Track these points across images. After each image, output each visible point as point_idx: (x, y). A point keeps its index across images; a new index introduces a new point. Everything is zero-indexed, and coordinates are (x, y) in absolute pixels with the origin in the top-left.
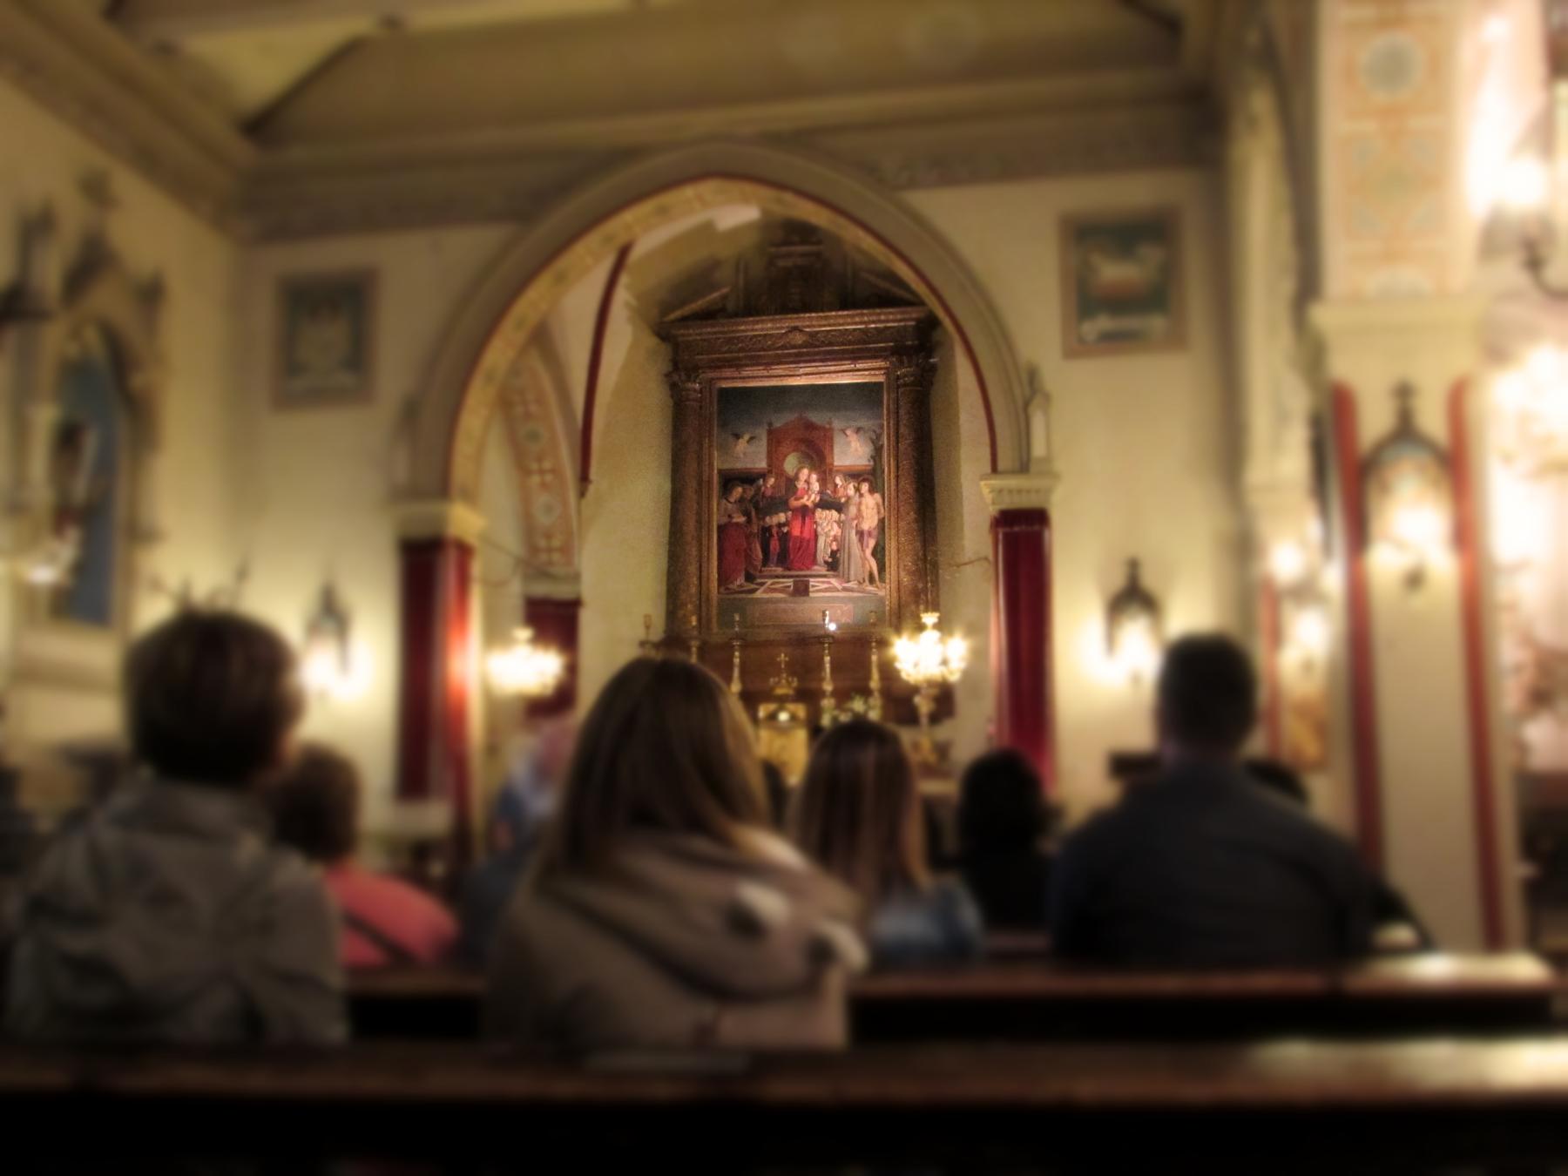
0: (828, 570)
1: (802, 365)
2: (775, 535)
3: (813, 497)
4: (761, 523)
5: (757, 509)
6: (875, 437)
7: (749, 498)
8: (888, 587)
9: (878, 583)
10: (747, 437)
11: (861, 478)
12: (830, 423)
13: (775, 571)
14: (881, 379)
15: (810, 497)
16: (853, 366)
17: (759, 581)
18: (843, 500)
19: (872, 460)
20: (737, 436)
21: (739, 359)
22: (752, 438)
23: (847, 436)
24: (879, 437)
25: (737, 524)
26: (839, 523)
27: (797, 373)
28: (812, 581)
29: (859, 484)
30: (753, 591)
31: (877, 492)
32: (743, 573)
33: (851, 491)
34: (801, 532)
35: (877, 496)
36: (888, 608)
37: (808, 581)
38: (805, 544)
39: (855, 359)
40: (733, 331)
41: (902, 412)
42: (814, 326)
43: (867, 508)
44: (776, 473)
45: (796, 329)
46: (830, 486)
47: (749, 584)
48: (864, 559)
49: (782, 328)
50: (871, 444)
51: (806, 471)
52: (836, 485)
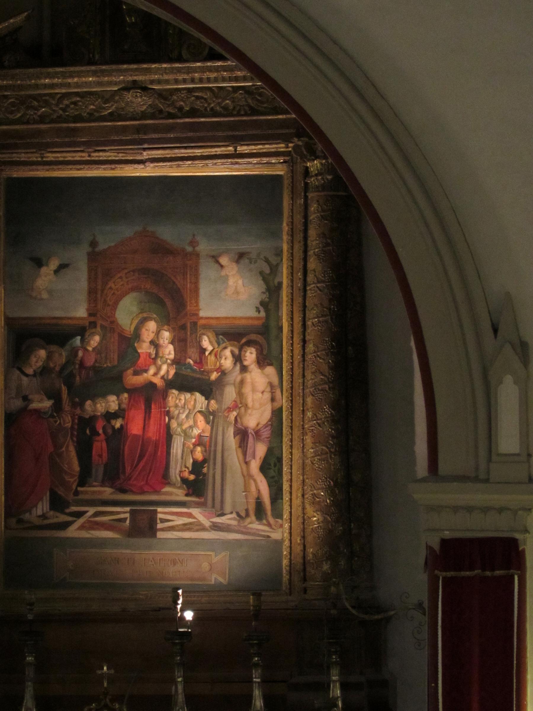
0: (187, 495)
1: (146, 146)
2: (101, 431)
3: (164, 368)
4: (78, 411)
5: (70, 386)
6: (267, 270)
7: (57, 369)
8: (287, 526)
9: (271, 520)
10: (54, 264)
11: (244, 340)
12: (193, 243)
13: (100, 492)
14: (280, 171)
15: (159, 369)
16: (231, 148)
17: (74, 509)
18: (214, 376)
19: (262, 309)
20: (39, 263)
21: (39, 133)
22: (62, 267)
23: (222, 266)
24: (275, 269)
25: (37, 411)
26: (207, 414)
27: (139, 158)
28: (162, 512)
29: (240, 350)
30: (65, 526)
31: (271, 364)
32: (47, 498)
33: (227, 362)
34: (144, 428)
35: (270, 370)
36: (285, 562)
37: (155, 512)
38: (150, 449)
39: (236, 140)
40: (30, 87)
41: (312, 233)
42: (167, 82)
43: (254, 390)
44: (102, 327)
45: (135, 86)
46: (193, 352)
47: (58, 514)
48: (248, 476)
49: (110, 83)
50: (261, 282)
51: (152, 325)
52: (203, 351)
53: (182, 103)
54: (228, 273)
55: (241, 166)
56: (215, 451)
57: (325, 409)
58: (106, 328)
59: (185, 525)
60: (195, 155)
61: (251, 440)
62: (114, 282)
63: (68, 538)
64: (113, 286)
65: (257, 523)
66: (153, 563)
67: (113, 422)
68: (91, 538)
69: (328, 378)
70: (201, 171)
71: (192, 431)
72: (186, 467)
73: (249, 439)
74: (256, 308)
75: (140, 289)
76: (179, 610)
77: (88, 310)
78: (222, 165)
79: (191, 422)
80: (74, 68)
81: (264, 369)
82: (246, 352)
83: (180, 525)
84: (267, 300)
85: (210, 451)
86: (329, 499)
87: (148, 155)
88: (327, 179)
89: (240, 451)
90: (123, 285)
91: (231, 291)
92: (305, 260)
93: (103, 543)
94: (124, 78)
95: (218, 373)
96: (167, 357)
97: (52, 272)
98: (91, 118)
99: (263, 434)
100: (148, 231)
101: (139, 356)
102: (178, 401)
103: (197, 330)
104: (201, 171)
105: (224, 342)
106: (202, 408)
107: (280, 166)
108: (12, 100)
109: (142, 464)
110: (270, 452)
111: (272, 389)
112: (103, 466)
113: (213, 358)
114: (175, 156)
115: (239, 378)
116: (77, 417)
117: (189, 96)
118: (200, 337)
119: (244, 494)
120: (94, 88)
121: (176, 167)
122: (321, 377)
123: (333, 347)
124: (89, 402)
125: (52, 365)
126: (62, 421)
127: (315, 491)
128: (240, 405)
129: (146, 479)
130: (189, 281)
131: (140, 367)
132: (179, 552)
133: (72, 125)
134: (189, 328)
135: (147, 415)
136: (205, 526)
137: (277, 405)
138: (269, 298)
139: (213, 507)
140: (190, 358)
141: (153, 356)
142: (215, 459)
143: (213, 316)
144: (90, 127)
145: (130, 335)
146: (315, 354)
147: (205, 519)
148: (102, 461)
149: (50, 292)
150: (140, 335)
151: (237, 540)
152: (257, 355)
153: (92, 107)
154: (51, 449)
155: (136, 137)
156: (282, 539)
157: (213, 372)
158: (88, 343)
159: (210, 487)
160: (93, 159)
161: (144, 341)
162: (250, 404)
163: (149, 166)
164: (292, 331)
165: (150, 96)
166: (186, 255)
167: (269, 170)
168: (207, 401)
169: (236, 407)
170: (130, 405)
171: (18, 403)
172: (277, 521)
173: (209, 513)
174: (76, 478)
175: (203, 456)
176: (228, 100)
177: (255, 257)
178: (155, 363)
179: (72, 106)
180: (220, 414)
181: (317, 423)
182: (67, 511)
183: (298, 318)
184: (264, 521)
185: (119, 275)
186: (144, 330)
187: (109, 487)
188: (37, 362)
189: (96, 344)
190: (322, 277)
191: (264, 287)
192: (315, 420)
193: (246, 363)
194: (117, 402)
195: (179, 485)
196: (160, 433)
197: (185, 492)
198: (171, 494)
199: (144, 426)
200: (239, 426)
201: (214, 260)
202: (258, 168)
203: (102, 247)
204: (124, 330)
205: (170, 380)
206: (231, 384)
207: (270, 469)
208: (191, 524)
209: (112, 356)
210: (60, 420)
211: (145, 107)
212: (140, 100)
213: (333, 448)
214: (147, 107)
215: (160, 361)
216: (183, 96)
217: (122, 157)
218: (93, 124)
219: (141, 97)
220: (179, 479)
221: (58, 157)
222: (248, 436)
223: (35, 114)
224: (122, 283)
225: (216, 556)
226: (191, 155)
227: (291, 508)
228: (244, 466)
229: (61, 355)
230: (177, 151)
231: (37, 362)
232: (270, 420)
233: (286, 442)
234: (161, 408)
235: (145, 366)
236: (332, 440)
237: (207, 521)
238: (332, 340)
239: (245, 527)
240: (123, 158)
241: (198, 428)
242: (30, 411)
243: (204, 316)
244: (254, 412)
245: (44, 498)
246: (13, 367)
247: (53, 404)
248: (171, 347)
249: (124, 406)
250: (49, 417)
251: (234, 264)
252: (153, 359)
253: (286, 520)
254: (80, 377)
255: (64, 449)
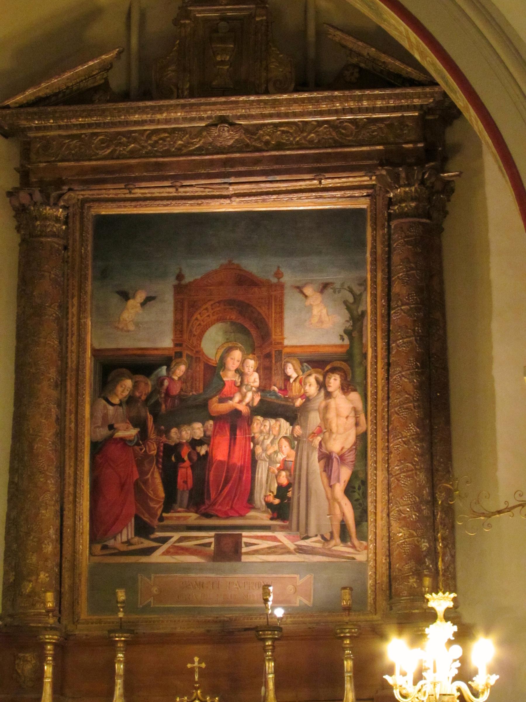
0: (272, 519)
1: (232, 180)
2: (186, 458)
3: (249, 395)
4: (164, 439)
6: (351, 300)
7: (144, 398)
9: (356, 542)
10: (141, 296)
11: (328, 367)
12: (278, 275)
13: (186, 518)
14: (363, 204)
15: (244, 396)
16: (316, 182)
18: (299, 402)
19: (346, 337)
20: (125, 296)
22: (149, 299)
23: (306, 297)
24: (358, 299)
25: (122, 440)
26: (291, 439)
27: (225, 193)
28: (247, 536)
29: (324, 377)
30: (149, 551)
31: (355, 390)
33: (312, 389)
35: (355, 396)
41: (396, 259)
42: (252, 117)
43: (338, 415)
44: (188, 356)
45: (223, 120)
46: (278, 379)
47: (143, 540)
48: (332, 500)
52: (288, 378)
53: (268, 138)
54: (312, 303)
55: (324, 200)
56: (300, 476)
57: (410, 427)
58: (192, 357)
59: (269, 548)
60: (280, 189)
61: (335, 464)
62: (200, 314)
63: (151, 564)
64: (199, 316)
65: (342, 545)
66: (238, 586)
67: (198, 449)
68: (175, 563)
69: (413, 397)
70: (285, 205)
71: (277, 456)
72: (270, 491)
73: (334, 463)
74: (341, 336)
75: (226, 319)
76: (269, 608)
77: (173, 340)
78: (306, 199)
79: (276, 447)
80: (163, 101)
81: (348, 395)
82: (330, 378)
83: (264, 549)
84: (351, 328)
85: (295, 475)
86: (415, 515)
87: (235, 190)
88: (410, 206)
89: (324, 474)
90: (209, 316)
91: (315, 320)
92: (389, 287)
93: (188, 568)
94: (211, 114)
95: (302, 400)
96: (252, 384)
97: (139, 305)
98: (179, 153)
99: (348, 457)
100: (233, 264)
101: (225, 384)
102: (262, 427)
103: (281, 357)
104: (285, 205)
105: (309, 369)
106: (286, 433)
107: (363, 199)
108: (101, 137)
109: (226, 490)
110: (354, 475)
111: (356, 415)
112: (188, 492)
113: (298, 384)
114: (261, 190)
115: (323, 404)
116: (162, 444)
117: (275, 130)
118: (284, 365)
119: (328, 517)
120: (181, 124)
121: (262, 202)
122: (406, 396)
123: (417, 367)
124: (174, 430)
125: (137, 394)
126: (147, 449)
127: (401, 508)
128: (325, 430)
129: (230, 504)
130: (273, 311)
131: (225, 395)
132: (265, 575)
133: (161, 160)
134: (273, 356)
135: (232, 441)
136: (290, 549)
137: (362, 429)
138: (353, 326)
139: (298, 529)
140: (275, 385)
141: (239, 384)
142: (299, 483)
143: (298, 344)
144: (178, 162)
145: (216, 364)
146: (400, 374)
147: (290, 542)
148: (187, 487)
149: (137, 324)
150: (225, 364)
151: (320, 562)
152: (341, 381)
153: (180, 142)
154: (136, 476)
155: (223, 170)
156: (367, 561)
157: (297, 398)
158: (174, 373)
159: (295, 511)
160: (180, 194)
161: (230, 370)
162: (334, 429)
163: (235, 201)
164: (376, 357)
165: (237, 131)
166: (270, 286)
167: (353, 203)
168: (291, 427)
169: (320, 432)
170: (215, 432)
171: (104, 432)
172: (361, 543)
173: (294, 536)
174: (161, 504)
175: (288, 480)
176: (313, 133)
177: (339, 287)
178: (240, 391)
179: (161, 142)
180: (305, 439)
181: (402, 440)
182: (152, 536)
183: (380, 344)
184: (349, 544)
185: (204, 307)
186: (229, 359)
187: (193, 512)
188: (123, 392)
189: (182, 373)
190: (407, 299)
191: (347, 315)
192: (400, 438)
193: (330, 390)
194: (202, 429)
195: (264, 509)
196: (245, 459)
197: (270, 516)
198: (256, 518)
199: (229, 452)
200: (324, 450)
201: (298, 290)
202: (342, 202)
203: (188, 279)
204: (210, 359)
205: (255, 406)
206: (316, 410)
207: (354, 492)
208: (276, 547)
209: (197, 385)
210: (146, 448)
211: (232, 142)
212: (227, 134)
213: (418, 465)
214: (234, 142)
215: (245, 389)
216: (269, 130)
217: (209, 192)
218: (181, 159)
219: (228, 131)
220: (264, 503)
221: (145, 193)
222: (333, 460)
223: (124, 149)
224: (207, 314)
225: (300, 578)
226: (276, 189)
227: (376, 529)
228: (328, 489)
229: (147, 384)
230: (263, 185)
231: (123, 392)
232: (355, 444)
233: (371, 465)
234: (246, 434)
235: (231, 394)
236: (417, 458)
237: (292, 544)
238: (417, 360)
239: (329, 549)
240: (209, 194)
241: (283, 453)
242: (116, 439)
243: (289, 345)
244: (339, 436)
245: (129, 524)
246: (99, 397)
247: (139, 432)
248: (256, 375)
249: (209, 433)
250: (134, 445)
251: (319, 294)
252: (238, 387)
253: (371, 540)
254: (166, 406)
255: (149, 476)
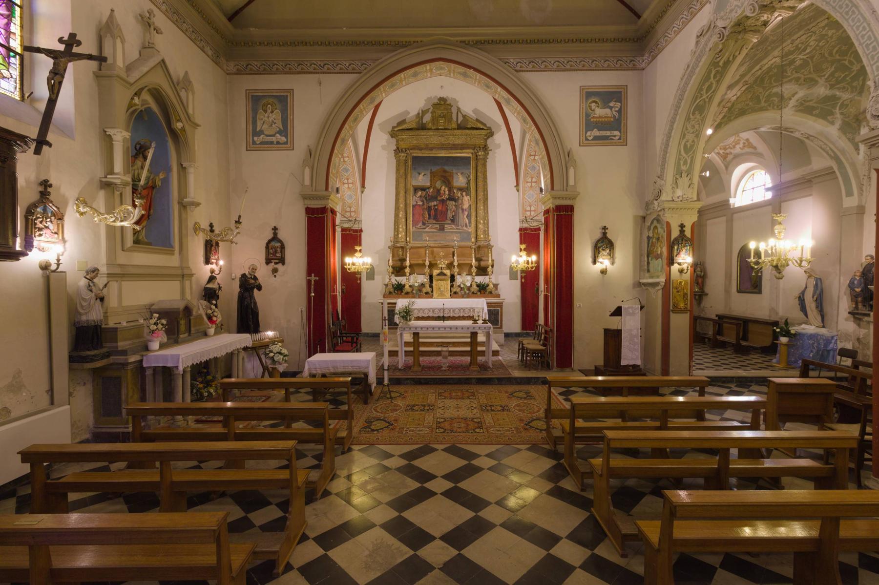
10: (423, 174)
20: (419, 174)
25: (419, 205)
26: (455, 205)
28: (446, 226)
33: (459, 195)
46: (452, 193)
51: (443, 187)
166: (450, 173)
